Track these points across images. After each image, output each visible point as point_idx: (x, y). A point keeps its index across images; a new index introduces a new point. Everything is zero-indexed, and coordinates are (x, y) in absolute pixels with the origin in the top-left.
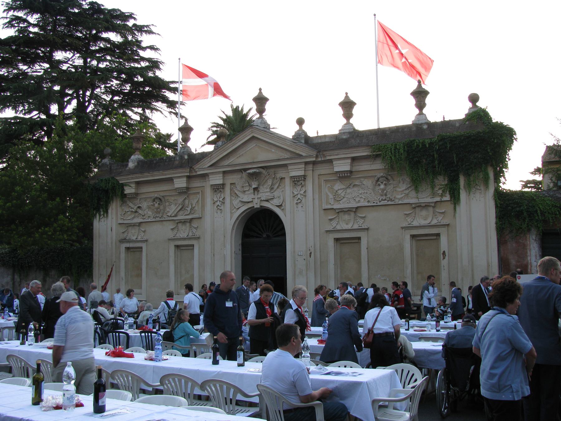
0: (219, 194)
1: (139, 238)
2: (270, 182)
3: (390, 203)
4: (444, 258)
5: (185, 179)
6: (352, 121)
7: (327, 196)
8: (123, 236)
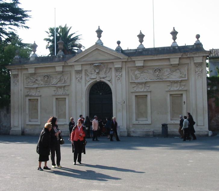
5: (143, 62)
8: (27, 94)
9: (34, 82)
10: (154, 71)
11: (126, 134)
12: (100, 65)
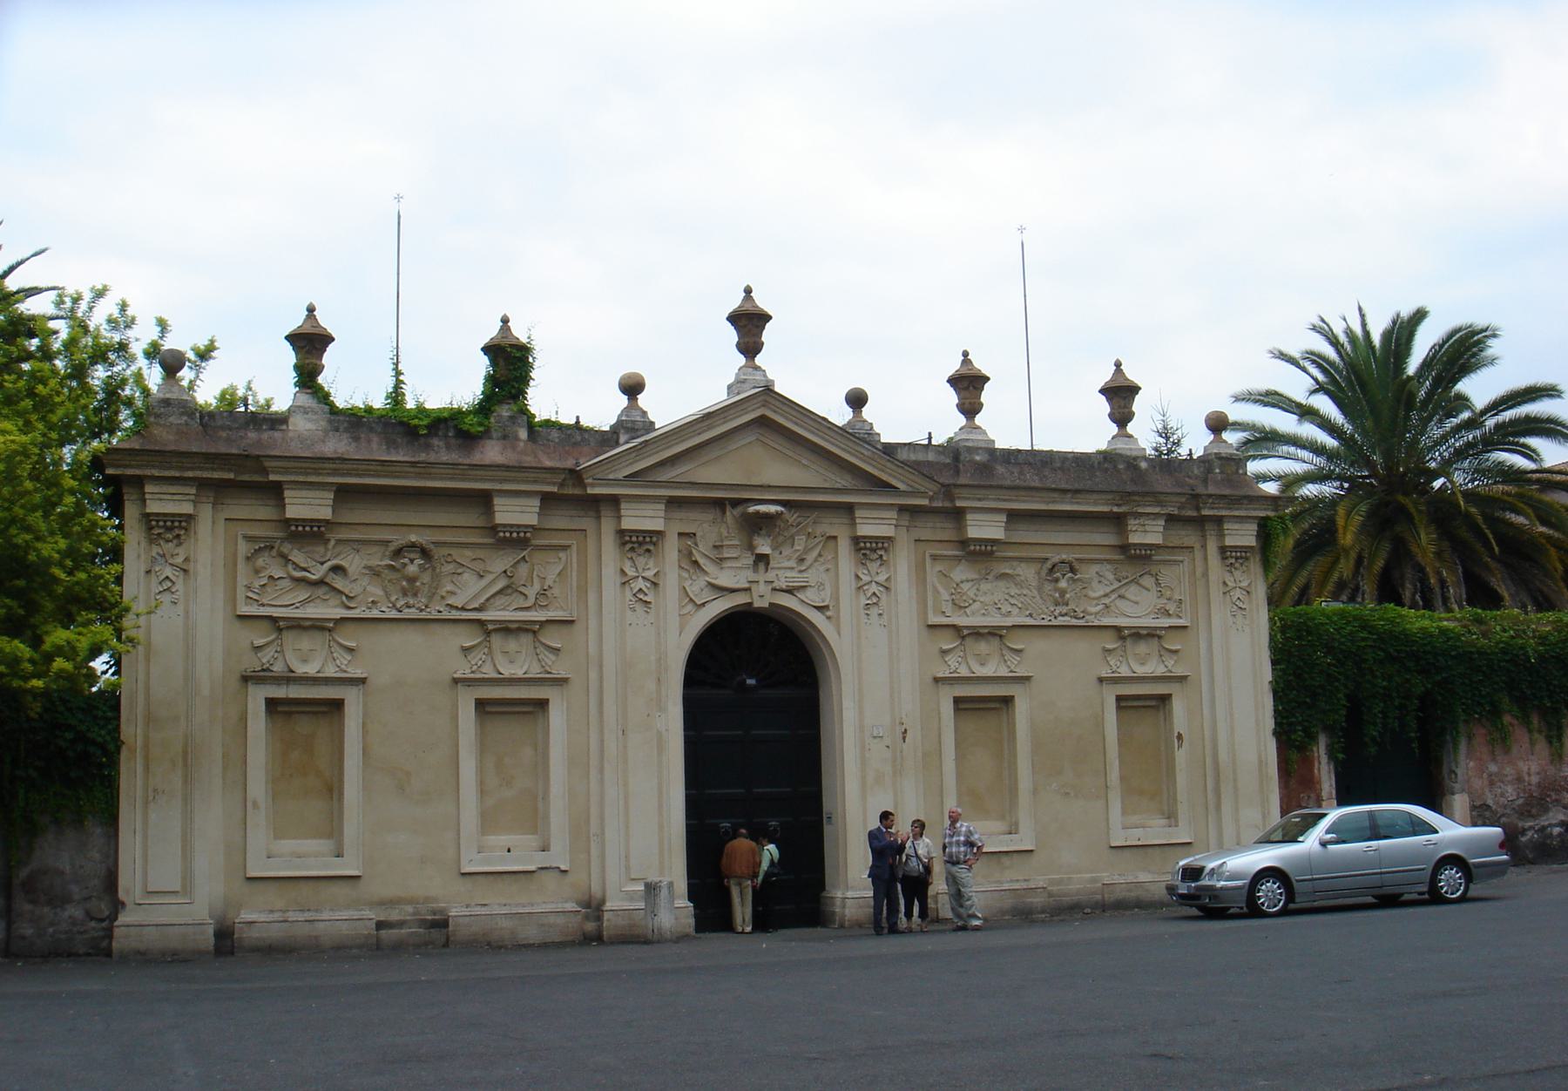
3: (1074, 622)
4: (1180, 746)
5: (536, 502)
6: (979, 420)
7: (936, 591)
8: (252, 663)
9: (321, 583)
10: (1044, 572)
11: (208, 938)
12: (779, 515)
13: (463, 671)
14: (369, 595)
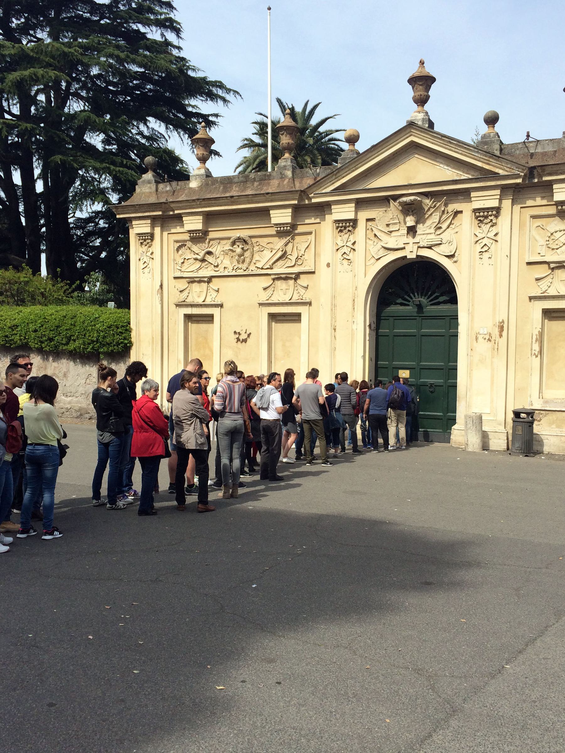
0: (347, 236)
1: (208, 302)
2: (435, 218)
13: (263, 299)
14: (227, 264)
